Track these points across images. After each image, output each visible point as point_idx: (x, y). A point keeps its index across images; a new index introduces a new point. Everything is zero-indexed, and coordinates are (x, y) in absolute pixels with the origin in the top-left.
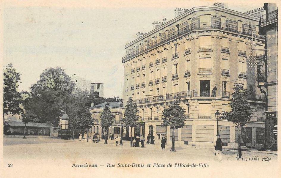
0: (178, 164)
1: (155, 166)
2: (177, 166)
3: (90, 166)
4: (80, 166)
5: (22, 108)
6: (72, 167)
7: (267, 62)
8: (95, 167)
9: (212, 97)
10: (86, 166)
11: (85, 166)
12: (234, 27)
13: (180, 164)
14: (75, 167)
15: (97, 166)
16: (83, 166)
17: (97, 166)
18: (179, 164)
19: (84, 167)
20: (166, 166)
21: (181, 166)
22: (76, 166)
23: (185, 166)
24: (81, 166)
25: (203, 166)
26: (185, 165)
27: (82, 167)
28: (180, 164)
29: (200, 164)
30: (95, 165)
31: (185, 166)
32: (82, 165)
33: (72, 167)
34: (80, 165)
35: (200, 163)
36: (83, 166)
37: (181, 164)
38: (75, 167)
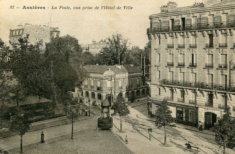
0: (104, 7)
1: (61, 8)
2: (103, 8)
3: (39, 8)
4: (29, 8)
5: (5, 129)
6: (23, 8)
7: (129, 77)
8: (43, 9)
9: (207, 114)
10: (35, 8)
11: (34, 8)
12: (204, 19)
13: (106, 7)
14: (26, 8)
15: (45, 8)
16: (33, 8)
17: (45, 8)
18: (105, 7)
19: (34, 9)
20: (94, 8)
21: (107, 8)
22: (26, 8)
23: (68, 8)
24: (31, 8)
25: (127, 8)
26: (68, 8)
27: (32, 9)
28: (106, 7)
29: (125, 7)
30: (43, 7)
31: (68, 8)
32: (32, 7)
33: (23, 8)
34: (30, 7)
35: (125, 6)
36: (33, 8)
37: (107, 7)
38: (26, 8)
